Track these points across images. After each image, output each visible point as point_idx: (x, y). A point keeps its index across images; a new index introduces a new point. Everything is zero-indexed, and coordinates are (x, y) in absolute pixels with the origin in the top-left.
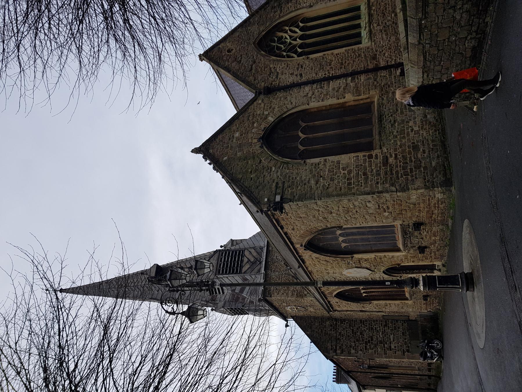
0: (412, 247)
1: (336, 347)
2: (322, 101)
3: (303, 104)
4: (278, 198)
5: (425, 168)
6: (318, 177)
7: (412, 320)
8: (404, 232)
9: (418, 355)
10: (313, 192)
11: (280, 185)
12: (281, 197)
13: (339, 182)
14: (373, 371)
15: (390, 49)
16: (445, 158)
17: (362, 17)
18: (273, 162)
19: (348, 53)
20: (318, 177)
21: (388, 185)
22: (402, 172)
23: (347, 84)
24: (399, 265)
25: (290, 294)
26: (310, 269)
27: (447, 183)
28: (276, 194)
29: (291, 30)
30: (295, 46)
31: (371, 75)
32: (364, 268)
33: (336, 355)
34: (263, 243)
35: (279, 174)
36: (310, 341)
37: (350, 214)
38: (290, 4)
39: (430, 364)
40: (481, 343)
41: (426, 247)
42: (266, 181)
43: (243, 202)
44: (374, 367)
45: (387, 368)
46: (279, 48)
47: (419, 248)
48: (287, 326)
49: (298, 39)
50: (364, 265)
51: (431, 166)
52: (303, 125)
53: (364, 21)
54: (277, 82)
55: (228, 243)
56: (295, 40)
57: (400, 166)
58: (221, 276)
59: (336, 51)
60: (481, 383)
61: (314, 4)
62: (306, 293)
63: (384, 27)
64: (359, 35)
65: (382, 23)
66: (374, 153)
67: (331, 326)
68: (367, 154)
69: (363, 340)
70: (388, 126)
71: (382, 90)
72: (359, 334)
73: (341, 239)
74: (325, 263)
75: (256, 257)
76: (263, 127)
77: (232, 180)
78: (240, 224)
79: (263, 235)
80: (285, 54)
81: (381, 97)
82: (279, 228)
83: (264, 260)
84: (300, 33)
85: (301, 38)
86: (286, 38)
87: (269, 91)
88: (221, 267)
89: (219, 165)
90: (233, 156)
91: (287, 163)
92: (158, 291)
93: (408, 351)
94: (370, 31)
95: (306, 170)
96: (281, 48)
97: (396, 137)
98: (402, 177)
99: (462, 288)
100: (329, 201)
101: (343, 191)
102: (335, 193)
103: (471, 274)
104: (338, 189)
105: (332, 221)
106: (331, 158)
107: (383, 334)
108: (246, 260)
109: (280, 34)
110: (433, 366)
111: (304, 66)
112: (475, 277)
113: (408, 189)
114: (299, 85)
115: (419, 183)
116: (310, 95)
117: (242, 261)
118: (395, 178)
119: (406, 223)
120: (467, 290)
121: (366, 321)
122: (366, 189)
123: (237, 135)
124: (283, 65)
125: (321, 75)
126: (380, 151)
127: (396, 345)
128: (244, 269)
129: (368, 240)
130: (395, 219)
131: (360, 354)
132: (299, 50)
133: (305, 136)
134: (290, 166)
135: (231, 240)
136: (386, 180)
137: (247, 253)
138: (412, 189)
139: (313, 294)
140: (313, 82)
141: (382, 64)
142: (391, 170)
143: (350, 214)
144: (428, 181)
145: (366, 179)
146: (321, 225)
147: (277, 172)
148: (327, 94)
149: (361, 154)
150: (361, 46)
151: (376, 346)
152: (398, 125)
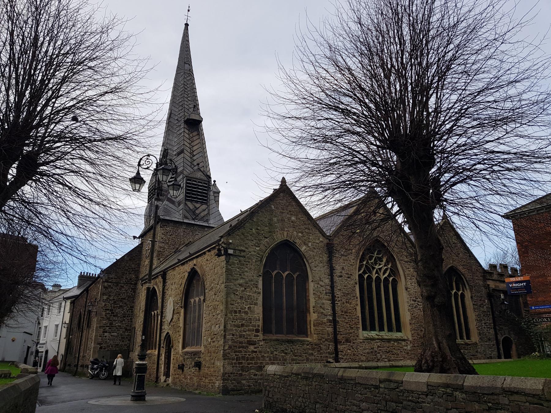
0: (184, 359)
1: (110, 282)
2: (314, 294)
3: (313, 277)
4: (230, 251)
5: (241, 375)
6: (245, 287)
7: (129, 354)
8: (196, 354)
9: (96, 356)
10: (232, 281)
11: (243, 254)
12: (231, 254)
13: (238, 303)
14: (86, 314)
15: (354, 355)
16: (248, 392)
17: (390, 333)
18: (263, 248)
19: (356, 318)
20: (245, 287)
21: (230, 343)
22: (240, 356)
23: (326, 315)
24: (172, 347)
25: (162, 245)
26: (177, 268)
27: (225, 391)
28: (234, 249)
29: (386, 270)
30: (370, 272)
31: (331, 336)
32: (173, 316)
33: (103, 282)
34: (212, 223)
35: (253, 253)
36: (118, 258)
37: (213, 310)
38: (412, 270)
39: (87, 366)
40: (92, 402)
41: (183, 371)
42: (247, 242)
43: (242, 213)
44: (90, 315)
45: (88, 327)
46: (371, 258)
47: (183, 365)
48: (135, 237)
49: (377, 275)
50: (175, 316)
51: (242, 380)
52: (295, 276)
53: (385, 334)
54: (337, 255)
55: (217, 189)
56: (377, 272)
57: (246, 355)
58: (185, 182)
59: (359, 308)
60: (63, 402)
61: (409, 291)
62: (161, 259)
63: (376, 352)
64: (373, 329)
65: (380, 350)
66: (260, 334)
67: (130, 279)
68: (260, 328)
69: (114, 307)
70: (283, 348)
71: (316, 345)
72: (121, 304)
73: (197, 299)
74: (180, 282)
75: (199, 216)
76: (297, 241)
77: (252, 212)
78: (232, 204)
79: (220, 223)
80: (365, 263)
81: (310, 343)
82: (209, 248)
83: (196, 223)
84: (382, 278)
85: (378, 279)
86: (380, 265)
87: (330, 249)
88: (194, 182)
89: (276, 193)
90: (274, 214)
91: (261, 261)
92: (177, 120)
93: (101, 348)
94: (373, 339)
95: (253, 276)
96: (371, 259)
97: (271, 353)
98: (236, 355)
99: (134, 392)
100: (223, 294)
101: (230, 306)
102: (229, 299)
103: (144, 400)
104: (232, 302)
105: (210, 294)
106: (261, 298)
107: (119, 326)
108: (198, 205)
109: (384, 260)
110: (85, 369)
111: (349, 279)
112: (142, 402)
113: (224, 360)
114: (331, 275)
115: (229, 369)
116: (321, 283)
117: (197, 202)
118: (237, 351)
119: (202, 356)
120: (132, 396)
121: (132, 312)
122: (229, 325)
123: (293, 218)
124: (352, 261)
125: (338, 294)
126: (261, 339)
127: (107, 338)
128: (189, 203)
129: (194, 322)
130: (205, 347)
131: (102, 304)
132: (366, 276)
133: (284, 277)
134: (258, 263)
135: (220, 192)
136: (235, 342)
137: (204, 207)
138: (224, 362)
139: (159, 266)
140: (332, 287)
141: (340, 347)
142: (243, 347)
143: (213, 310)
144: (229, 376)
145: (238, 326)
146: (207, 284)
147: (254, 252)
148: (319, 298)
149: (260, 323)
150: (361, 330)
151: (108, 319)
152: (282, 356)
